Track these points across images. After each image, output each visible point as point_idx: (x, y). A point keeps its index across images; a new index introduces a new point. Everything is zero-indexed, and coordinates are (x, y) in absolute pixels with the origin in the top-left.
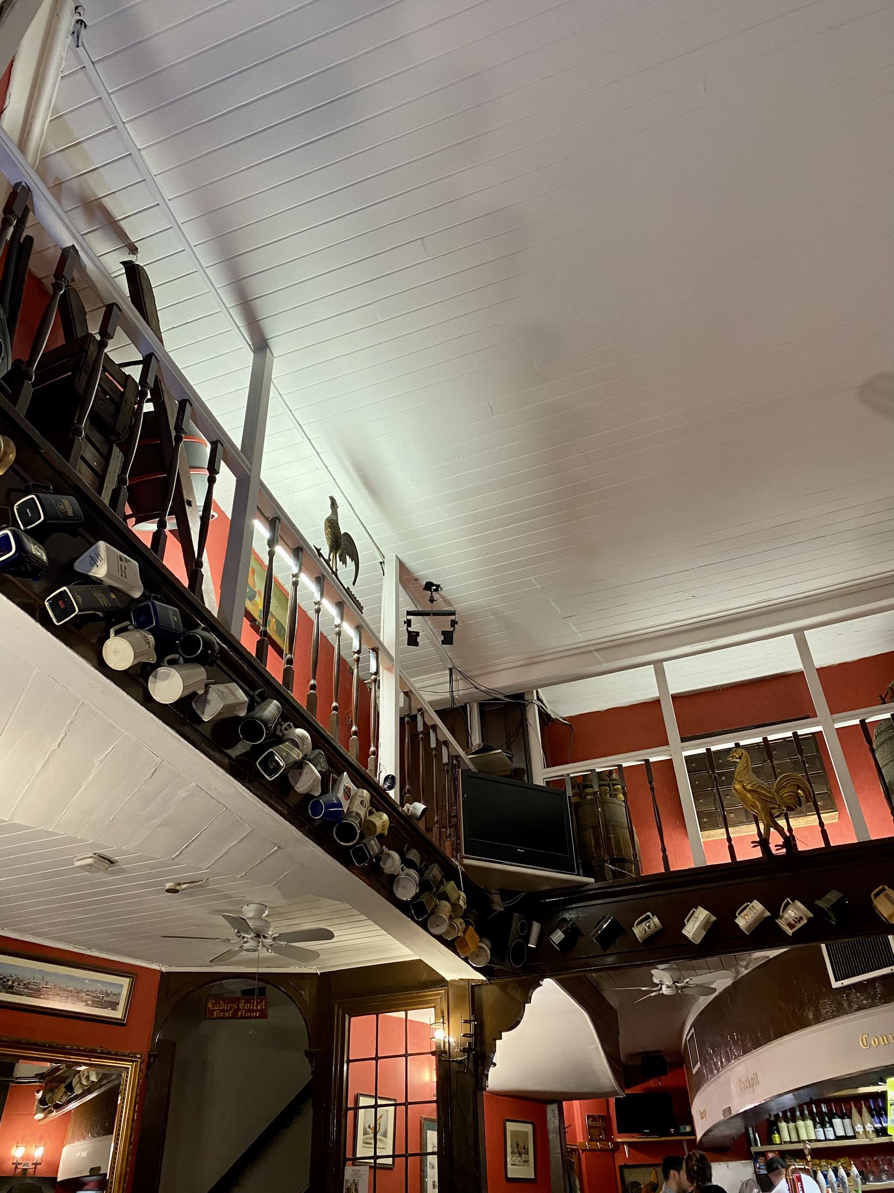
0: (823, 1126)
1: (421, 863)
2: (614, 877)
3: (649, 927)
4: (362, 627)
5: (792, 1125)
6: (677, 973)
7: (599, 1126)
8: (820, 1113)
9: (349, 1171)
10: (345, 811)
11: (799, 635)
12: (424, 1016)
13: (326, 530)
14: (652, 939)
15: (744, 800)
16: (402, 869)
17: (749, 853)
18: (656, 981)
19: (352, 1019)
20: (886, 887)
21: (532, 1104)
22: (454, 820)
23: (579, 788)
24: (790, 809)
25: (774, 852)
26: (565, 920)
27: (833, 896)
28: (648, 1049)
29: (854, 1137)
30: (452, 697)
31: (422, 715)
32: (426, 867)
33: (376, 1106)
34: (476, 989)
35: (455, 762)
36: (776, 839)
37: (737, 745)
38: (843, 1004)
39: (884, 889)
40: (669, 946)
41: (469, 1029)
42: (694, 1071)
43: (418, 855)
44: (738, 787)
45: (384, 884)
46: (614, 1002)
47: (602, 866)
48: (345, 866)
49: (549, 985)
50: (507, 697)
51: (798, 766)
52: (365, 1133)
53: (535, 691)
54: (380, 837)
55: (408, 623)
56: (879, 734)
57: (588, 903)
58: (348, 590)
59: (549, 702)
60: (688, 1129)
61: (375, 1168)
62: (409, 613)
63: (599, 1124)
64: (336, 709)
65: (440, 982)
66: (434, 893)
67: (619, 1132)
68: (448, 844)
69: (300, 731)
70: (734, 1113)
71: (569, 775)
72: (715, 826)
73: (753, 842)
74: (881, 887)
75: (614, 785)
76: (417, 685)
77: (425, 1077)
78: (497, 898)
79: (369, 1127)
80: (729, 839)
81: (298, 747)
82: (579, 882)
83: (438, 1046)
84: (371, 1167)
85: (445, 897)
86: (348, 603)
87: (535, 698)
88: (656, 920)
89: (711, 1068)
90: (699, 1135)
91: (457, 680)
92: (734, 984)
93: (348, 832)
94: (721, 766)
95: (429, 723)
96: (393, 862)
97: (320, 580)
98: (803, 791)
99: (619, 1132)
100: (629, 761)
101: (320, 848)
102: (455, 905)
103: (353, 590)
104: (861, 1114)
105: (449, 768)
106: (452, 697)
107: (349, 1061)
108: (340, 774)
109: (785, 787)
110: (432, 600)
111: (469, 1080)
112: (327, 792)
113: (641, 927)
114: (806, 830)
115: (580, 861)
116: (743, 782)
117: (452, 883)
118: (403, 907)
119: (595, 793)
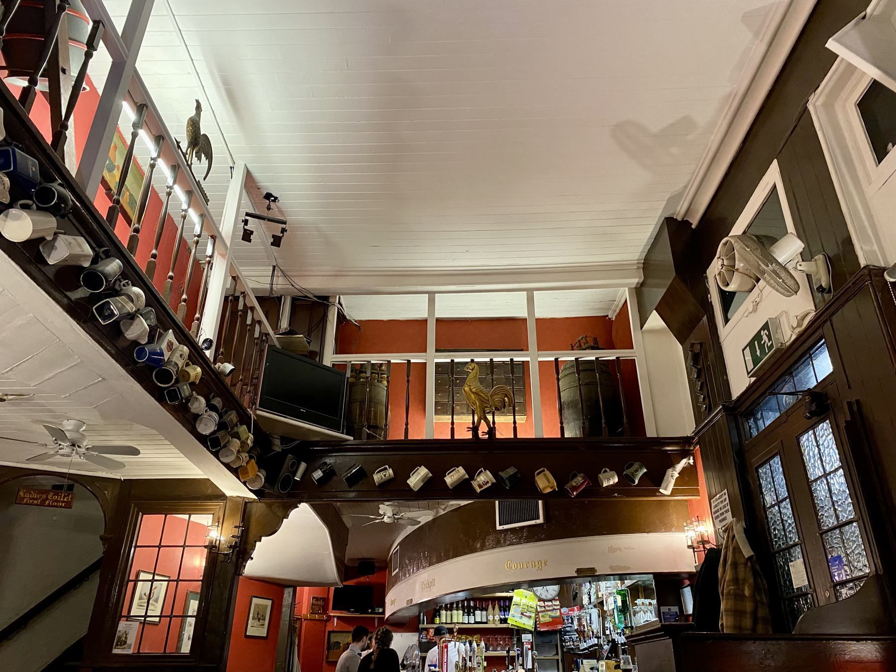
0: (469, 615)
5: (449, 613)
6: (397, 509)
7: (320, 605)
9: (122, 625)
11: (530, 292)
12: (204, 519)
15: (469, 398)
17: (463, 434)
18: (381, 512)
21: (274, 587)
22: (255, 381)
24: (497, 409)
26: (325, 463)
27: (511, 471)
29: (486, 623)
30: (272, 288)
31: (244, 297)
32: (226, 412)
33: (153, 581)
34: (249, 505)
36: (483, 428)
38: (501, 540)
40: (397, 490)
41: (237, 532)
42: (393, 574)
44: (467, 389)
45: (190, 421)
47: (361, 429)
50: (315, 296)
51: (508, 381)
52: (141, 598)
54: (192, 384)
55: (246, 222)
56: (565, 369)
58: (198, 183)
59: (347, 307)
60: (381, 610)
61: (144, 623)
62: (247, 214)
64: (171, 278)
65: (221, 496)
69: (136, 290)
70: (414, 603)
72: (445, 413)
76: (244, 273)
77: (197, 562)
85: (237, 436)
86: (197, 194)
88: (391, 471)
90: (387, 615)
93: (165, 376)
94: (459, 373)
95: (249, 305)
96: (199, 404)
100: (396, 359)
102: (244, 444)
103: (203, 184)
105: (259, 342)
106: (272, 288)
107: (136, 546)
108: (166, 330)
109: (497, 394)
110: (269, 208)
111: (231, 569)
113: (379, 475)
114: (503, 425)
116: (472, 385)
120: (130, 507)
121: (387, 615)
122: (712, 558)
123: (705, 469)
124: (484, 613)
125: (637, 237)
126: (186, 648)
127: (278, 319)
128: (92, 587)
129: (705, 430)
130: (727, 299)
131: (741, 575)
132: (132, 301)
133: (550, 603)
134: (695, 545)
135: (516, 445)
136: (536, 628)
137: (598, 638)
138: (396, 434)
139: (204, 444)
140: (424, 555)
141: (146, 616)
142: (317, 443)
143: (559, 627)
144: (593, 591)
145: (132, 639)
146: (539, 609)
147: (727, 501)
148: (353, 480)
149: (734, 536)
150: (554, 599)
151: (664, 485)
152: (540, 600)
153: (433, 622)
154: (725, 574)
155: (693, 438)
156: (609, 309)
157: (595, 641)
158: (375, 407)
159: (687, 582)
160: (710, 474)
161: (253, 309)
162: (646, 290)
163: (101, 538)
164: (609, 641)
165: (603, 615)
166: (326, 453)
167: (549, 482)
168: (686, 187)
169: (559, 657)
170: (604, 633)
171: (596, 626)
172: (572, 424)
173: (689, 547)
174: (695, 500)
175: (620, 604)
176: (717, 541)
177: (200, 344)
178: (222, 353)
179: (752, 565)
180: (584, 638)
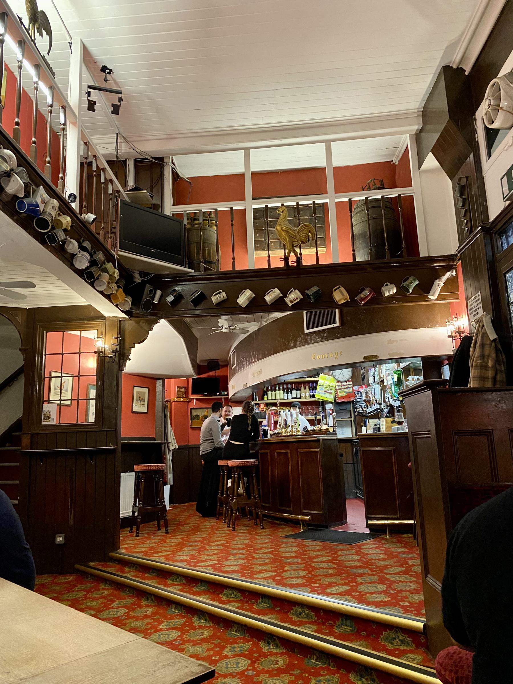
0: (287, 393)
1: (91, 250)
2: (205, 270)
4: (54, 88)
5: (273, 392)
6: (231, 322)
7: (184, 391)
8: (287, 388)
9: (45, 406)
10: (42, 211)
11: (328, 143)
12: (90, 334)
13: (26, 4)
14: (220, 304)
15: (280, 235)
16: (79, 252)
17: (278, 264)
18: (220, 325)
19: (48, 333)
21: (149, 380)
22: (114, 230)
24: (303, 243)
25: (290, 265)
26: (175, 290)
27: (315, 289)
28: (212, 358)
29: (300, 398)
30: (117, 153)
31: (96, 160)
32: (95, 253)
33: (61, 377)
34: (122, 322)
35: (116, 194)
36: (292, 258)
37: (282, 205)
38: (308, 340)
39: (339, 287)
40: (228, 307)
41: (117, 341)
42: (232, 368)
43: (90, 245)
44: (278, 228)
45: (69, 259)
46: (197, 335)
47: (199, 264)
48: (42, 244)
49: (163, 323)
50: (153, 158)
51: (311, 220)
52: (55, 389)
53: (171, 157)
54: (65, 230)
55: (89, 94)
56: (357, 208)
57: (189, 283)
58: (43, 57)
59: (179, 166)
60: (226, 393)
61: (60, 405)
62: (89, 87)
64: (34, 143)
65: (101, 317)
66: (99, 268)
68: (109, 242)
69: (8, 152)
70: (248, 386)
71: (186, 211)
72: (263, 249)
75: (211, 220)
76: (95, 142)
77: (91, 363)
78: (137, 276)
79: (58, 387)
80: (269, 257)
81: (6, 162)
83: (99, 349)
84: (58, 405)
85: (106, 270)
86: (42, 66)
87: (171, 162)
88: (224, 294)
90: (230, 395)
91: (121, 142)
93: (43, 223)
94: (272, 217)
95: (101, 167)
96: (73, 246)
97: (21, 43)
98: (312, 234)
100: (222, 207)
101: (24, 231)
102: (111, 276)
103: (46, 57)
104: (305, 389)
105: (112, 197)
106: (117, 153)
107: (46, 355)
108: (38, 186)
109: (303, 231)
110: (106, 80)
111: (116, 367)
112: (29, 197)
113: (216, 297)
114: (308, 255)
115: (187, 260)
116: (282, 224)
117: (111, 264)
118: (80, 273)
119: (200, 224)
121: (230, 397)
122: (466, 343)
123: (465, 279)
124: (298, 392)
125: (417, 87)
126: (92, 419)
127: (126, 179)
128: (21, 382)
129: (466, 247)
130: (492, 135)
131: (487, 353)
132: (6, 161)
133: (345, 384)
134: (454, 335)
135: (319, 270)
136: (335, 400)
137: (380, 404)
138: (226, 267)
139: (82, 276)
140: (253, 353)
141: (61, 400)
142: (168, 276)
143: (352, 399)
144: (377, 373)
145: (54, 415)
146: (337, 388)
147: (480, 300)
148: (196, 302)
149: (483, 326)
152: (338, 382)
153: (263, 399)
154: (474, 353)
155: (456, 255)
156: (393, 155)
157: (378, 406)
159: (446, 362)
160: (468, 282)
161: (104, 170)
162: (423, 135)
163: (21, 350)
164: (388, 406)
165: (384, 389)
166: (176, 283)
167: (343, 295)
168: (461, 35)
169: (353, 419)
170: (384, 401)
171: (379, 397)
173: (449, 337)
174: (456, 302)
175: (396, 380)
176: (470, 329)
177: (67, 198)
178: (85, 207)
179: (495, 345)
180: (370, 405)
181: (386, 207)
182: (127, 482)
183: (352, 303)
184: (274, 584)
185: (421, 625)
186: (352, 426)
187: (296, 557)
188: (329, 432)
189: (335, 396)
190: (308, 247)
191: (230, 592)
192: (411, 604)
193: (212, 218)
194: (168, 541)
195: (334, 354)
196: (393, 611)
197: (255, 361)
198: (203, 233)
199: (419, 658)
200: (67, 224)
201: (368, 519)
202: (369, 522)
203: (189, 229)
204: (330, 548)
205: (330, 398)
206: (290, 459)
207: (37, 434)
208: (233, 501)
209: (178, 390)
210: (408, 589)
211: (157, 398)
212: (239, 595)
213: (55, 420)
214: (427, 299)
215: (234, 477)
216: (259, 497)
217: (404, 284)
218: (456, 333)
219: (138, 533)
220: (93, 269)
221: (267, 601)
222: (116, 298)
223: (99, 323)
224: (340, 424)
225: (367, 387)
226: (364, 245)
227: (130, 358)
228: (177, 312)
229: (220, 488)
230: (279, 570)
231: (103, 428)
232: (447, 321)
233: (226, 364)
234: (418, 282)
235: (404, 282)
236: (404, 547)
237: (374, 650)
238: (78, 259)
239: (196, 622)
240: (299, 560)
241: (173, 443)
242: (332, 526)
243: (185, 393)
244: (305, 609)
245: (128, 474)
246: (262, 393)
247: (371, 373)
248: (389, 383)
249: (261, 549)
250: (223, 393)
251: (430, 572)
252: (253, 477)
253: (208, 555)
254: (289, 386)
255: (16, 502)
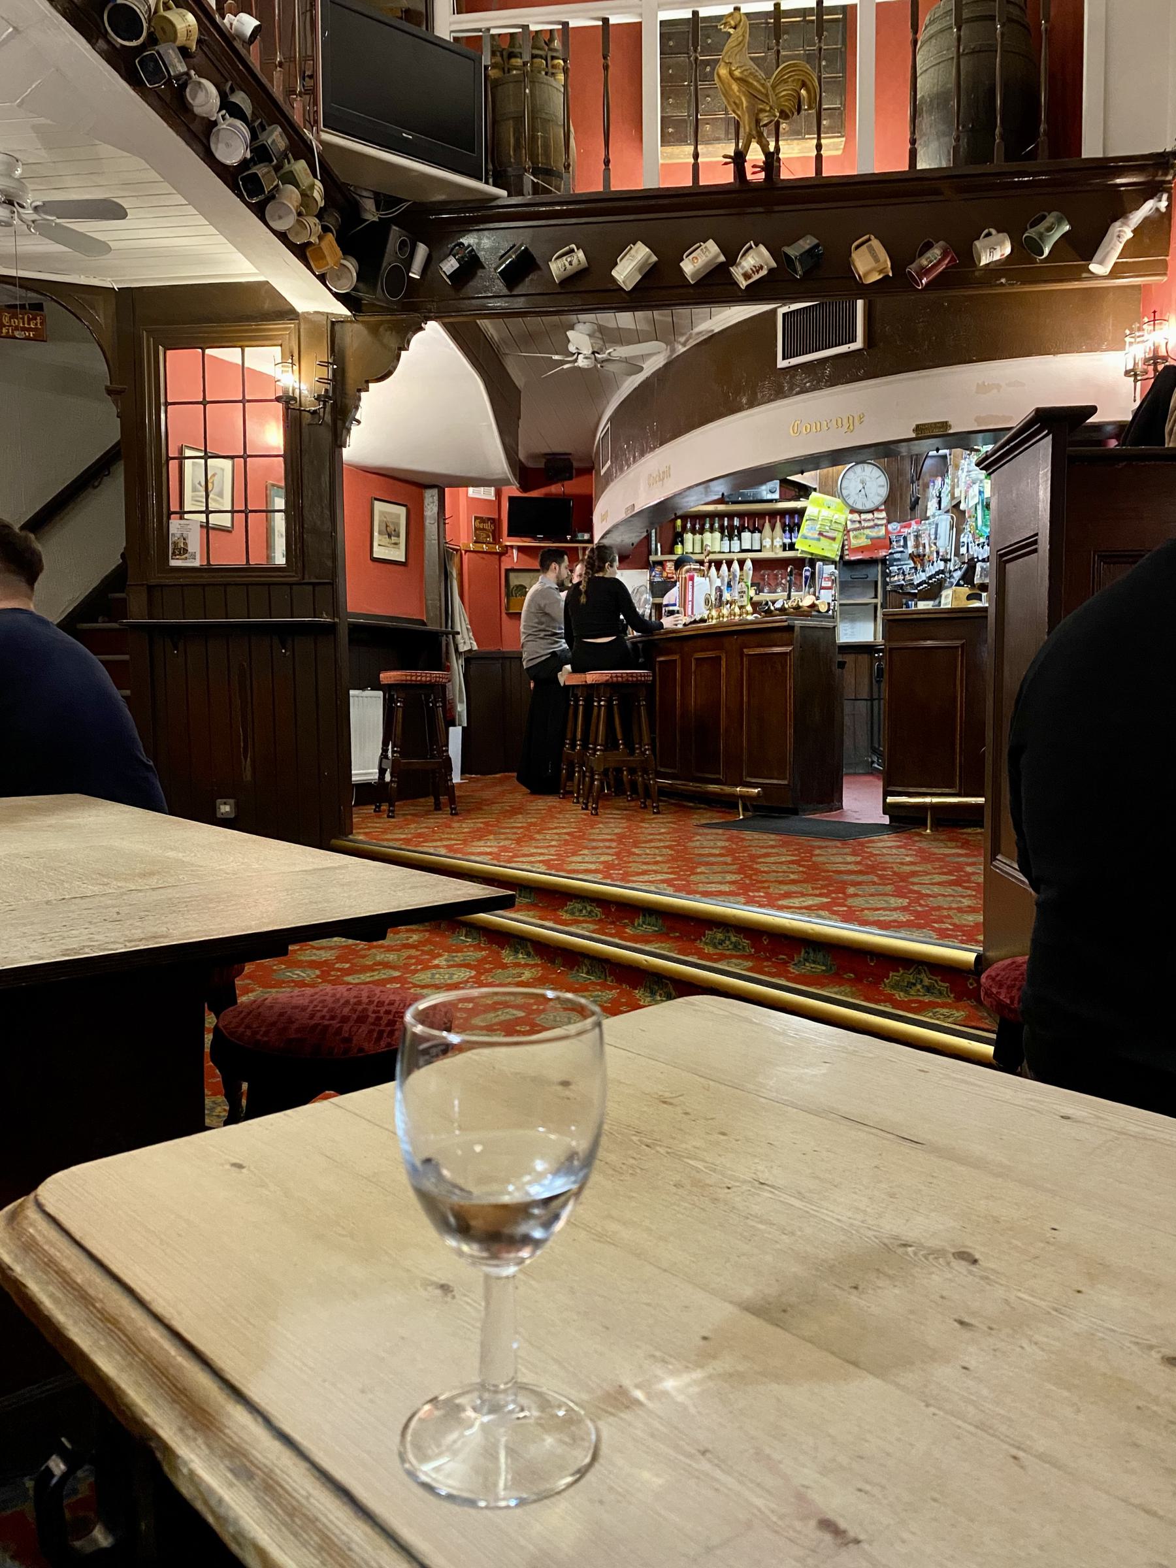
3: (570, 263)
5: (698, 537)
7: (488, 527)
8: (731, 527)
9: (175, 525)
14: (573, 280)
16: (223, 117)
17: (720, 175)
18: (572, 348)
19: (169, 352)
20: (993, 231)
21: (409, 486)
22: (309, 83)
23: (502, 56)
24: (784, 115)
25: (749, 177)
27: (807, 243)
29: (760, 551)
34: (337, 327)
36: (755, 155)
38: (782, 386)
39: (869, 240)
40: (591, 291)
45: (199, 134)
46: (519, 380)
47: (520, 177)
49: (433, 330)
52: (194, 490)
54: (184, 51)
56: (932, 22)
60: (586, 536)
61: (206, 527)
63: (488, 526)
65: (289, 313)
67: (509, 535)
70: (637, 510)
71: (488, 30)
72: (682, 141)
73: (725, 157)
74: (866, 237)
75: (553, 58)
77: (271, 435)
78: (369, 205)
82: (486, 193)
83: (286, 391)
88: (580, 254)
89: (621, 461)
90: (596, 541)
92: (665, 366)
96: (206, 97)
99: (509, 535)
102: (306, 195)
104: (773, 529)
107: (167, 404)
109: (785, 81)
111: (326, 435)
113: (560, 263)
114: (796, 156)
115: (490, 167)
116: (732, 65)
120: (141, 338)
124: (757, 535)
126: (280, 560)
133: (870, 516)
136: (841, 557)
137: (946, 561)
138: (586, 181)
142: (442, 207)
143: (883, 553)
145: (195, 544)
146: (850, 526)
150: (877, 509)
151: (1097, 257)
152: (853, 511)
153: (672, 552)
157: (941, 565)
158: (545, 131)
167: (877, 260)
169: (879, 601)
170: (957, 554)
171: (944, 544)
172: (934, 145)
173: (1127, 373)
181: (1010, 20)
182: (366, 711)
183: (898, 281)
184: (670, 890)
185: (971, 957)
186: (876, 617)
187: (721, 855)
188: (819, 611)
189: (843, 546)
190: (797, 134)
191: (579, 906)
192: (957, 927)
193: (555, 50)
194: (456, 825)
195: (845, 421)
196: (916, 934)
197: (655, 448)
198: (531, 91)
199: (959, 1014)
200: (189, 32)
201: (886, 794)
202: (890, 799)
203: (496, 80)
204: (798, 844)
205: (832, 550)
206: (723, 670)
207: (162, 586)
208: (594, 754)
209: (478, 525)
210: (954, 905)
211: (427, 532)
212: (598, 910)
213: (198, 556)
214: (1084, 275)
215: (600, 706)
216: (653, 750)
217: (1031, 233)
218: (1146, 361)
219: (393, 811)
220: (261, 170)
221: (653, 920)
222: (321, 256)
223: (285, 329)
224: (850, 612)
225: (919, 523)
226: (942, 127)
227: (357, 417)
228: (467, 302)
229: (569, 736)
230: (684, 870)
231: (306, 576)
232: (1128, 332)
233: (588, 469)
234: (1067, 228)
235: (1031, 227)
236: (961, 847)
237: (867, 1000)
238: (222, 133)
239: (507, 956)
240: (729, 859)
241: (466, 636)
242: (805, 811)
243: (493, 533)
244: (730, 934)
245: (369, 693)
246: (670, 536)
247: (933, 492)
248: (972, 503)
249: (651, 841)
250: (580, 537)
251: (1003, 848)
252: (639, 706)
253: (536, 847)
254: (736, 522)
255: (128, 692)
